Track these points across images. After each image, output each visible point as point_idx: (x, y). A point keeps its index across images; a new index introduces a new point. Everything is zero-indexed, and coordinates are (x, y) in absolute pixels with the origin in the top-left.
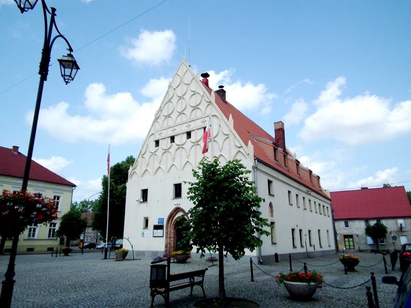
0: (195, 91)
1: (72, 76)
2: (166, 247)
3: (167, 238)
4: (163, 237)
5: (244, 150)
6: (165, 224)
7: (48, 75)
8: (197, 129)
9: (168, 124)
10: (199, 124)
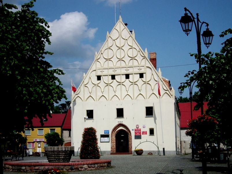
0: (132, 46)
1: (210, 42)
2: (112, 148)
3: (111, 143)
4: (109, 142)
5: (170, 93)
6: (110, 134)
7: (197, 41)
8: (134, 74)
9: (19, 159)
10: (136, 70)
